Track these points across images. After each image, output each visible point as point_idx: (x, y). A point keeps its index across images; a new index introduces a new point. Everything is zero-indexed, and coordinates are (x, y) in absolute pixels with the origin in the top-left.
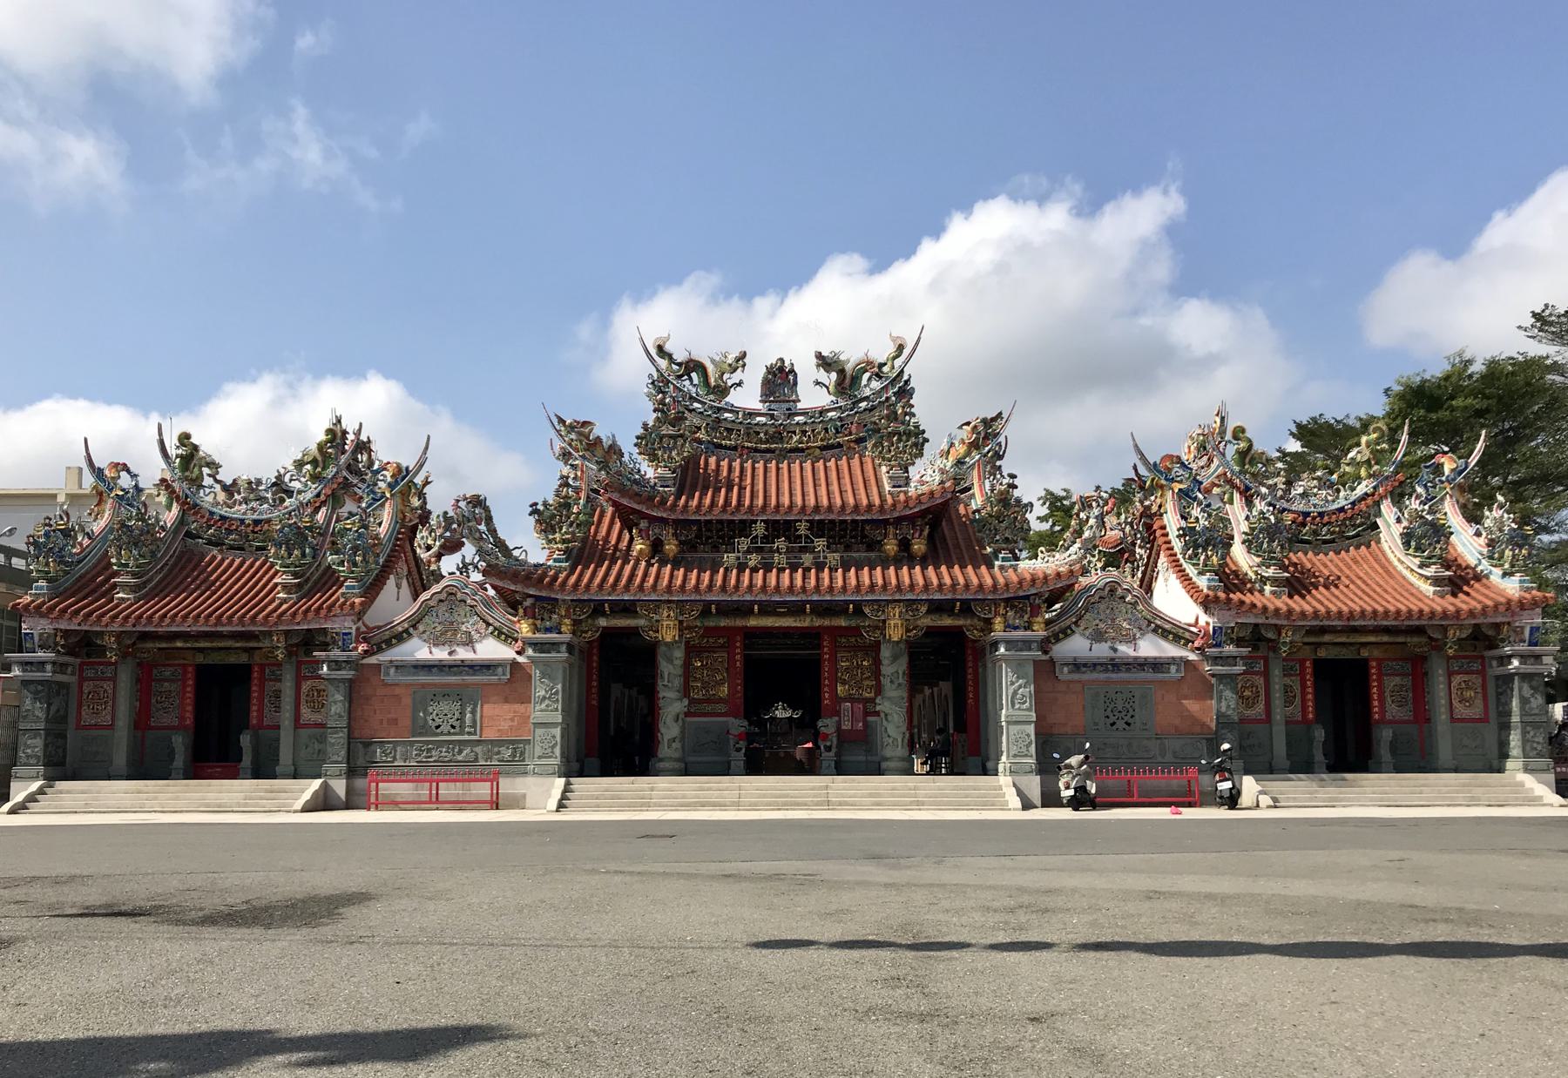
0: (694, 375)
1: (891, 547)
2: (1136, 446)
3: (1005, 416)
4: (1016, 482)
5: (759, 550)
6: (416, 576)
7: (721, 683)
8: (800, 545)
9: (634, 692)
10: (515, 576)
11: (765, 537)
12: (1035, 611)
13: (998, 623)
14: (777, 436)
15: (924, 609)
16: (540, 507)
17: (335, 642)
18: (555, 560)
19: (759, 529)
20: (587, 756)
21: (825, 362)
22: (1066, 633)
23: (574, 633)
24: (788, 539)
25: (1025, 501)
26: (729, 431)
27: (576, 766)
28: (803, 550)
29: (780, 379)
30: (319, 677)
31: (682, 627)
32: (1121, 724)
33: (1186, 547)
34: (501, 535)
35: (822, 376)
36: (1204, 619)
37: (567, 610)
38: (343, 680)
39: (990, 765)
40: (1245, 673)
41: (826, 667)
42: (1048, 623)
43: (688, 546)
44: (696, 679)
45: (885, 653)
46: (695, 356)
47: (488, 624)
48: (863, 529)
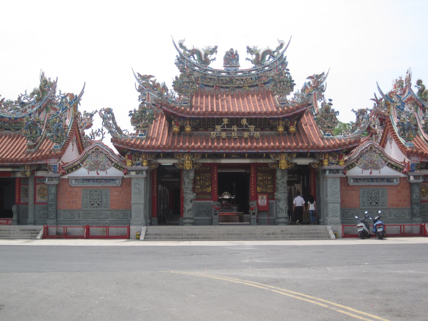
0: (195, 56)
1: (281, 129)
2: (378, 87)
3: (325, 74)
4: (332, 102)
5: (225, 130)
6: (79, 141)
7: (208, 186)
8: (243, 129)
9: (165, 188)
10: (122, 143)
11: (227, 125)
12: (341, 157)
13: (326, 163)
14: (231, 81)
15: (295, 156)
16: (133, 112)
17: (50, 169)
18: (140, 135)
19: (226, 121)
20: (152, 217)
21: (250, 51)
22: (352, 166)
23: (148, 165)
24: (237, 126)
25: (336, 111)
26: (211, 79)
27: (149, 221)
28: (244, 130)
29: (231, 57)
30: (44, 184)
31: (194, 164)
32: (96, 205)
33: (401, 130)
34: (119, 125)
35: (250, 56)
36: (407, 160)
37: (146, 156)
38: (54, 185)
39: (321, 220)
40: (423, 182)
41: (252, 180)
42: (346, 161)
43: (195, 128)
44: (197, 185)
45: (279, 174)
46: (196, 48)
47: (112, 162)
48: (269, 122)
